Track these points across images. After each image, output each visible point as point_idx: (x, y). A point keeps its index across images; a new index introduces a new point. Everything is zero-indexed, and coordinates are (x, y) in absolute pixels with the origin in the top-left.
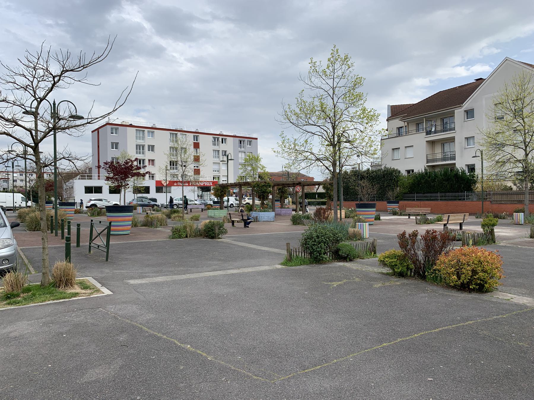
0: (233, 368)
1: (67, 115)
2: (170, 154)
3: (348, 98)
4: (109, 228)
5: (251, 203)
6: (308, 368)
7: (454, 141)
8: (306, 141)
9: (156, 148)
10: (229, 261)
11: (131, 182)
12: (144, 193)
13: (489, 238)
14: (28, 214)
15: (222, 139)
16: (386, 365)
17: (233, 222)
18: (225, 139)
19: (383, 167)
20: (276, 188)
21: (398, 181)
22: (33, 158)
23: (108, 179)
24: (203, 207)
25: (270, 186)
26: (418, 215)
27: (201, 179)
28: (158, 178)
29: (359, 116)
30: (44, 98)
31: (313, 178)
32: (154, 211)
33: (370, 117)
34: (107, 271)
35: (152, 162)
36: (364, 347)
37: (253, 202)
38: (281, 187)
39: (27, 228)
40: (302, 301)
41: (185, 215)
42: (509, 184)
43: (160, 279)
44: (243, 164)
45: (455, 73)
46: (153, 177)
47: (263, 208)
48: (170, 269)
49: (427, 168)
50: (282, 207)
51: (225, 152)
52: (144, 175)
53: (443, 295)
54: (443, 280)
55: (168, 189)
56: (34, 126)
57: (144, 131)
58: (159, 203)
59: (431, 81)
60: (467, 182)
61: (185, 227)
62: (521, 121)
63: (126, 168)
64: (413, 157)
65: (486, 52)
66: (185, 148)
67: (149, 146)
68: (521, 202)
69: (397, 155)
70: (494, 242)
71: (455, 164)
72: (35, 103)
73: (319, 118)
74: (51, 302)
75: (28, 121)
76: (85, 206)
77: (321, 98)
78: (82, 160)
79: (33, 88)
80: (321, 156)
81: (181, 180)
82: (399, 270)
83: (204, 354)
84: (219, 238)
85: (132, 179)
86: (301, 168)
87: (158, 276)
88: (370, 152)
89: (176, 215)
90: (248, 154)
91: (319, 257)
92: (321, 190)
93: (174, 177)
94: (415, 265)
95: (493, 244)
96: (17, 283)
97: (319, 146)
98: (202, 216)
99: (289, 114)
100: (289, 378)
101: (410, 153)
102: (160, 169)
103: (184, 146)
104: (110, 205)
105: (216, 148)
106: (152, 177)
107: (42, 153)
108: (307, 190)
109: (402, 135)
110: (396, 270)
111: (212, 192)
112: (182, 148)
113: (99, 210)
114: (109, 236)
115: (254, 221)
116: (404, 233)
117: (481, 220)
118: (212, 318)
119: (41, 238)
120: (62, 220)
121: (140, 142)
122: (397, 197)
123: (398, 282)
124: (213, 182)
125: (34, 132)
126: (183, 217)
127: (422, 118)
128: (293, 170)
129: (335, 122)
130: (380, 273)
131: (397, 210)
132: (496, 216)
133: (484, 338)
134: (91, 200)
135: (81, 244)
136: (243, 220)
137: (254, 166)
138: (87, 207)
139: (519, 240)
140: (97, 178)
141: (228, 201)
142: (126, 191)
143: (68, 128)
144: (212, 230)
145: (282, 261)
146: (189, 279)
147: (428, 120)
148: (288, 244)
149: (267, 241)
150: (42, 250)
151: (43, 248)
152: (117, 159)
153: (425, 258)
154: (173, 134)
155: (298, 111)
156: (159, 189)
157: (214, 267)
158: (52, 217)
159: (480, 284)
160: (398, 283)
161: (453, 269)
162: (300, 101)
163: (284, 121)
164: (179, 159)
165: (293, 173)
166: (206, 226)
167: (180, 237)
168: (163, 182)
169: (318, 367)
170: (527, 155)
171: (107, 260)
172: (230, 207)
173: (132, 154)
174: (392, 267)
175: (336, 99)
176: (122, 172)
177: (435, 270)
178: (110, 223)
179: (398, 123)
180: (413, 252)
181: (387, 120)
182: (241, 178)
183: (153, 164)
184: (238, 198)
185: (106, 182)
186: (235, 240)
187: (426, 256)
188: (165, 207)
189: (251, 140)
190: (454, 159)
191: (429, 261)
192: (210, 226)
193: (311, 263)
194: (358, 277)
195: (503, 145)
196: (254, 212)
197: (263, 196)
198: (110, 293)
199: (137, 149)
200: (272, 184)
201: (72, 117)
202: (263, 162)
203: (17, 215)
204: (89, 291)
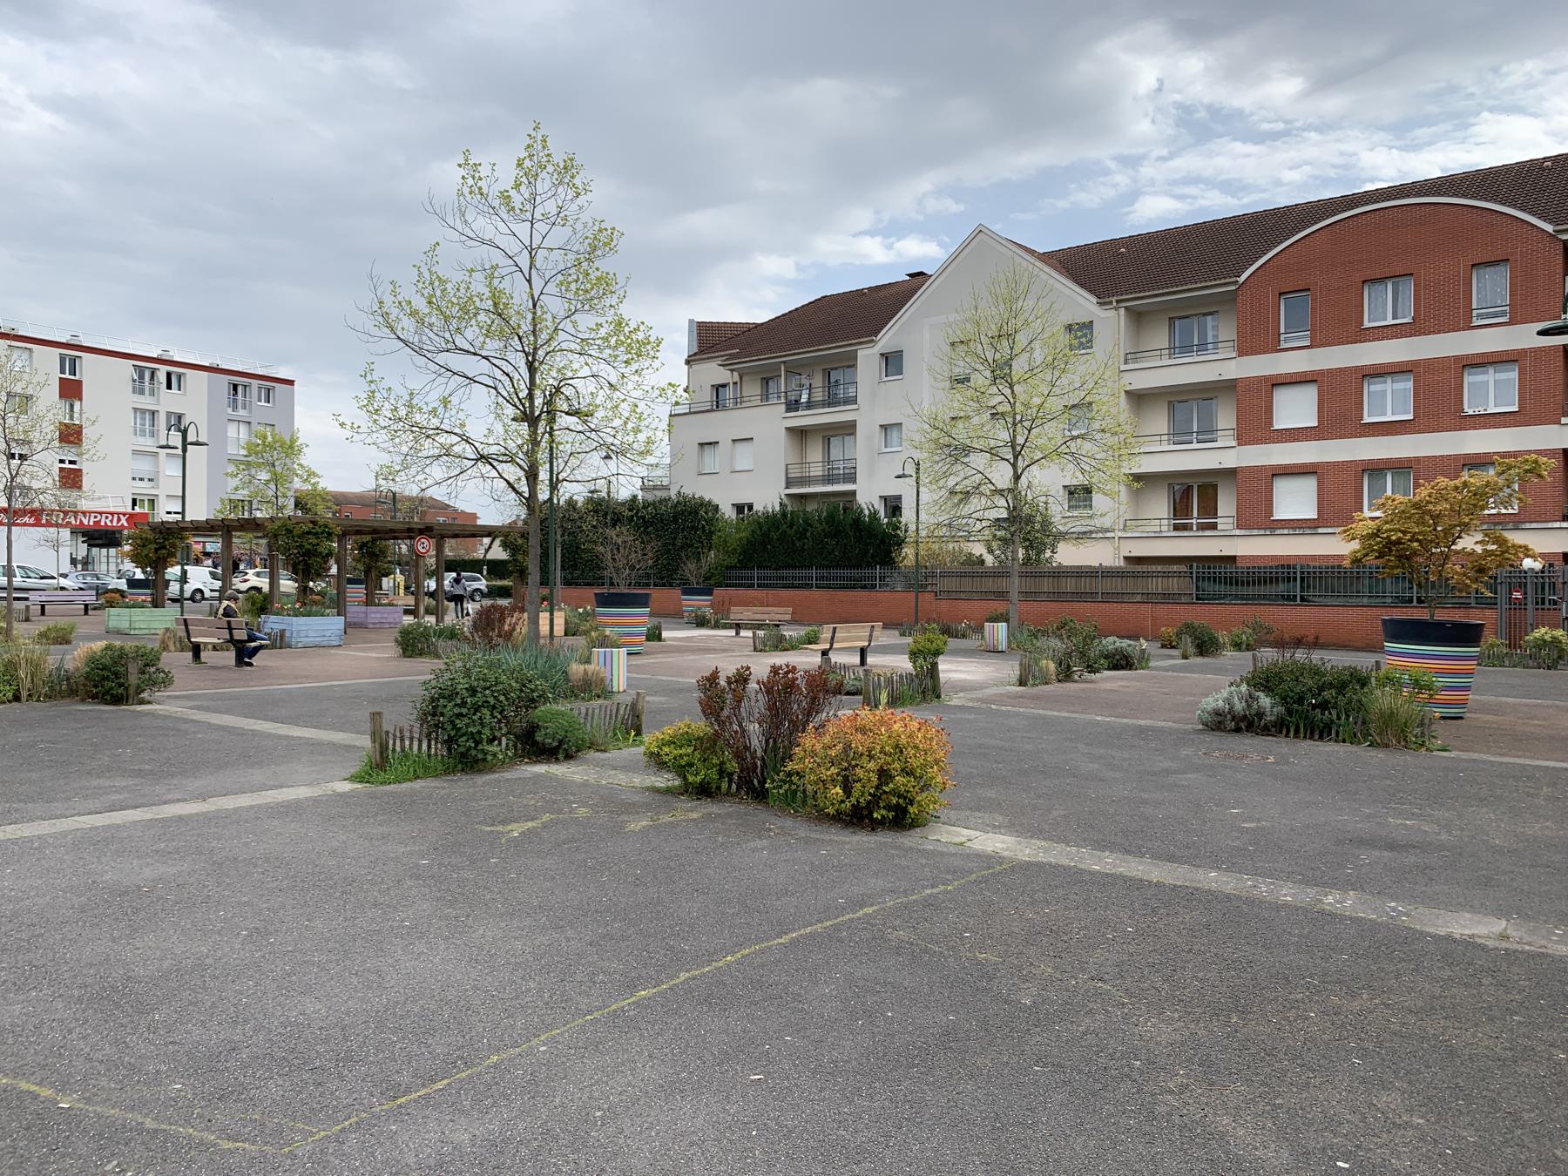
0: (149, 1124)
3: (573, 286)
5: (266, 588)
6: (407, 1092)
7: (853, 433)
8: (445, 402)
13: (926, 686)
15: (169, 375)
16: (640, 1053)
17: (196, 650)
18: (179, 377)
19: (673, 494)
21: (712, 533)
24: (90, 597)
25: (330, 534)
26: (759, 627)
27: (84, 505)
29: (605, 339)
31: (474, 516)
33: (639, 348)
36: (584, 1007)
38: (368, 538)
40: (410, 888)
41: (15, 625)
42: (978, 549)
44: (241, 462)
45: (860, 255)
47: (304, 604)
49: (785, 500)
50: (369, 601)
51: (180, 417)
53: (807, 841)
54: (810, 801)
59: (799, 268)
60: (883, 542)
62: (1007, 391)
64: (751, 472)
65: (933, 206)
66: (28, 398)
68: (1002, 595)
69: (712, 460)
70: (938, 697)
71: (854, 493)
73: (488, 334)
77: (491, 272)
80: (494, 449)
82: (698, 779)
83: (46, 1092)
84: (142, 702)
86: (430, 482)
88: (635, 446)
91: (474, 752)
92: (498, 553)
94: (741, 763)
95: (935, 702)
97: (485, 419)
98: (81, 631)
99: (395, 312)
100: (343, 1130)
101: (744, 457)
103: (18, 389)
105: (146, 402)
108: (451, 550)
109: (725, 408)
110: (691, 779)
115: (273, 647)
116: (714, 676)
117: (910, 640)
118: (91, 965)
122: (707, 578)
123: (694, 811)
124: (131, 517)
127: (777, 367)
128: (408, 487)
129: (535, 349)
130: (648, 789)
131: (708, 612)
132: (947, 631)
133: (898, 951)
136: (231, 640)
137: (279, 469)
139: (994, 690)
141: (184, 579)
146: (14, 842)
147: (793, 370)
148: (376, 717)
153: (767, 741)
155: (420, 304)
157: (115, 797)
159: (897, 808)
160: (695, 815)
161: (834, 770)
162: (426, 274)
163: (375, 331)
166: (92, 660)
169: (440, 1085)
170: (1017, 477)
172: (192, 599)
174: (681, 770)
175: (538, 283)
177: (790, 774)
179: (715, 372)
180: (736, 727)
181: (688, 362)
182: (234, 504)
184: (219, 571)
187: (770, 737)
189: (272, 384)
190: (852, 478)
191: (775, 749)
192: (107, 661)
193: (449, 771)
194: (583, 804)
195: (967, 450)
196: (273, 618)
197: (306, 565)
200: (338, 530)
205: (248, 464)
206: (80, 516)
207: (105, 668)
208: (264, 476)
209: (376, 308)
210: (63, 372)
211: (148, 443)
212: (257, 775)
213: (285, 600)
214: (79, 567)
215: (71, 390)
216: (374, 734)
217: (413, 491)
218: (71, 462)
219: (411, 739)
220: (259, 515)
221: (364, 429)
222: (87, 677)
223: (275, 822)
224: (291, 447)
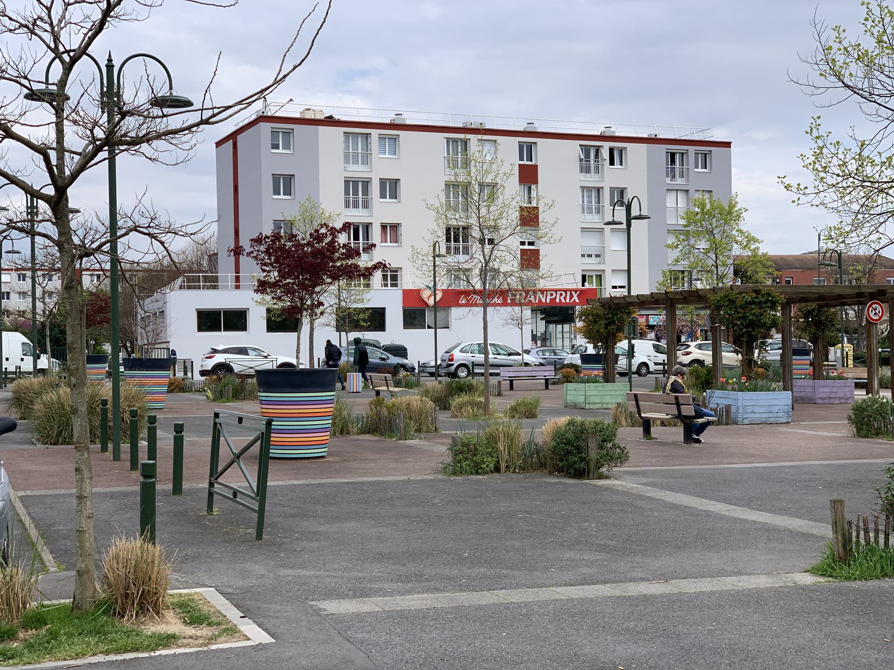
1: (143, 98)
2: (449, 207)
4: (265, 438)
9: (403, 188)
10: (635, 553)
11: (330, 295)
12: (368, 329)
14: (38, 394)
15: (611, 151)
18: (621, 151)
20: (794, 310)
22: (52, 230)
23: (263, 286)
27: (542, 284)
28: (411, 279)
30: (83, 51)
32: (397, 384)
34: (258, 570)
35: (392, 230)
37: (716, 356)
38: (812, 306)
39: (36, 435)
43: (417, 601)
46: (394, 278)
47: (749, 378)
48: (447, 572)
51: (622, 192)
52: (367, 273)
55: (440, 315)
56: (53, 136)
57: (367, 136)
58: (412, 360)
61: (492, 439)
63: (316, 253)
66: (494, 186)
67: (383, 182)
72: (57, 69)
74: (100, 658)
75: (38, 122)
76: (197, 369)
78: (186, 235)
79: (51, 24)
81: (479, 286)
84: (601, 477)
85: (333, 288)
86: (884, 242)
87: (409, 592)
89: (465, 398)
90: (698, 196)
93: (457, 278)
96: (8, 599)
98: (545, 404)
99: (840, 59)
102: (415, 253)
103: (489, 179)
104: (269, 366)
105: (592, 180)
106: (392, 277)
107: (78, 211)
111: (579, 324)
112: (481, 185)
113: (238, 381)
114: (264, 461)
115: (719, 423)
119: (73, 466)
120: (134, 414)
121: (358, 171)
124: (582, 293)
125: (53, 155)
126: (485, 406)
128: (858, 247)
134: (215, 351)
135: (185, 486)
136: (680, 416)
138: (203, 373)
140: (231, 283)
142: (317, 322)
143: (147, 139)
144: (579, 449)
145: (816, 560)
146: (507, 606)
148: (837, 505)
149: (765, 489)
150: (75, 501)
151: (80, 497)
152: (291, 224)
154: (455, 141)
155: (869, 44)
156: (414, 317)
157: (585, 570)
158: (104, 403)
162: (876, 11)
163: (821, 82)
164: (473, 221)
165: (857, 259)
166: (558, 435)
167: (477, 469)
168: (425, 294)
171: (259, 536)
172: (638, 372)
173: (335, 210)
176: (304, 265)
178: (269, 423)
182: (675, 276)
183: (395, 239)
184: (663, 343)
185: (259, 297)
186: (653, 485)
188: (432, 374)
189: (709, 150)
192: (570, 436)
196: (718, 393)
197: (747, 337)
198: (266, 638)
199: (347, 192)
200: (782, 298)
201: (159, 102)
202: (749, 223)
203: (9, 395)
204: (205, 631)
205: (687, 234)
206: (539, 294)
207: (568, 443)
208: (703, 245)
209: (820, 56)
210: (521, 159)
211: (594, 220)
212: (715, 560)
213: (728, 373)
214: (539, 342)
215: (528, 175)
216: (835, 524)
217: (864, 251)
218: (531, 244)
219: (877, 532)
220: (699, 285)
221: (811, 190)
222: (554, 450)
223: (738, 612)
224: (730, 213)
